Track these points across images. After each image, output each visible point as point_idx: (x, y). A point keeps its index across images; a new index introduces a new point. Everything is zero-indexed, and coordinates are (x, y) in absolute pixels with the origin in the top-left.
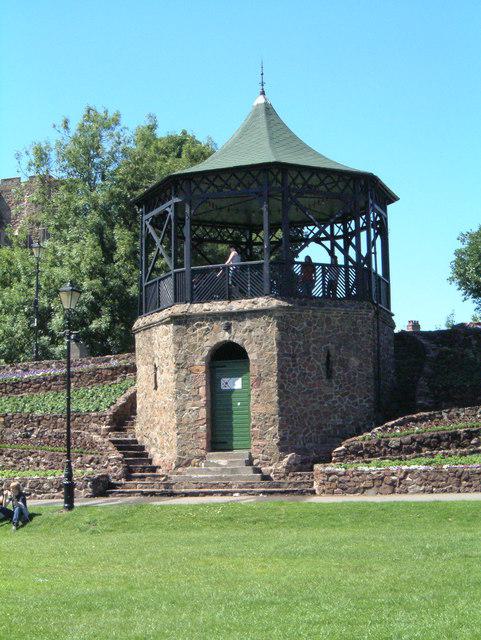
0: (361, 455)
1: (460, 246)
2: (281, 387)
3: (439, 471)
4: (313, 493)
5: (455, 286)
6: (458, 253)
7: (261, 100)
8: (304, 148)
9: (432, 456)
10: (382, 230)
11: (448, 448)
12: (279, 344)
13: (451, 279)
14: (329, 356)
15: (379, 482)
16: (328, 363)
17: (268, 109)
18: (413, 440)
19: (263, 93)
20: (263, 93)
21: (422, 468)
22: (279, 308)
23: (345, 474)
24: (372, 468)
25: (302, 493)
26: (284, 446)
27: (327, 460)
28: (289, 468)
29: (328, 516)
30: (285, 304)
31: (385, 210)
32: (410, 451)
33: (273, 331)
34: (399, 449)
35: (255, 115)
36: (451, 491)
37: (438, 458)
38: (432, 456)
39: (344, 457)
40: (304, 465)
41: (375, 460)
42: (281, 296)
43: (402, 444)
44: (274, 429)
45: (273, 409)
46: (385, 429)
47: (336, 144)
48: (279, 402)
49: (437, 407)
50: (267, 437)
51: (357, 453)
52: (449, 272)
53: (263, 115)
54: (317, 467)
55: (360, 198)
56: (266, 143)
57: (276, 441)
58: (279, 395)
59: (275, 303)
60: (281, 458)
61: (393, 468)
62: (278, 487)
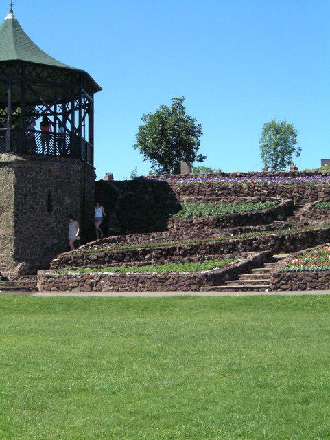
0: (70, 264)
1: (144, 124)
2: (16, 216)
3: (123, 277)
4: (37, 290)
5: (138, 151)
6: (141, 128)
7: (9, 16)
8: (31, 46)
9: (119, 266)
10: (90, 110)
11: (129, 261)
12: (16, 187)
13: (136, 146)
14: (49, 195)
15: (82, 283)
16: (49, 201)
17: (15, 23)
18: (106, 255)
19: (12, 12)
20: (12, 12)
21: (112, 274)
22: (16, 161)
23: (59, 277)
24: (77, 273)
25: (29, 290)
26: (17, 257)
27: (47, 267)
28: (20, 273)
29: (46, 306)
30: (19, 158)
31: (92, 97)
32: (103, 262)
33: (11, 177)
34: (94, 260)
35: (5, 26)
36: (131, 290)
37: (122, 267)
38: (119, 266)
39: (58, 266)
40: (31, 271)
41: (79, 268)
42: (11, 151)
43: (98, 257)
44: (11, 245)
45: (10, 231)
46: (87, 247)
47: (61, 49)
48: (15, 227)
49: (124, 233)
50: (6, 251)
51: (67, 263)
52: (134, 141)
53: (10, 27)
54: (40, 272)
55: (76, 87)
56: (12, 46)
57: (12, 254)
58: (15, 222)
59: (13, 158)
60: (15, 266)
61: (92, 274)
62: (13, 285)
